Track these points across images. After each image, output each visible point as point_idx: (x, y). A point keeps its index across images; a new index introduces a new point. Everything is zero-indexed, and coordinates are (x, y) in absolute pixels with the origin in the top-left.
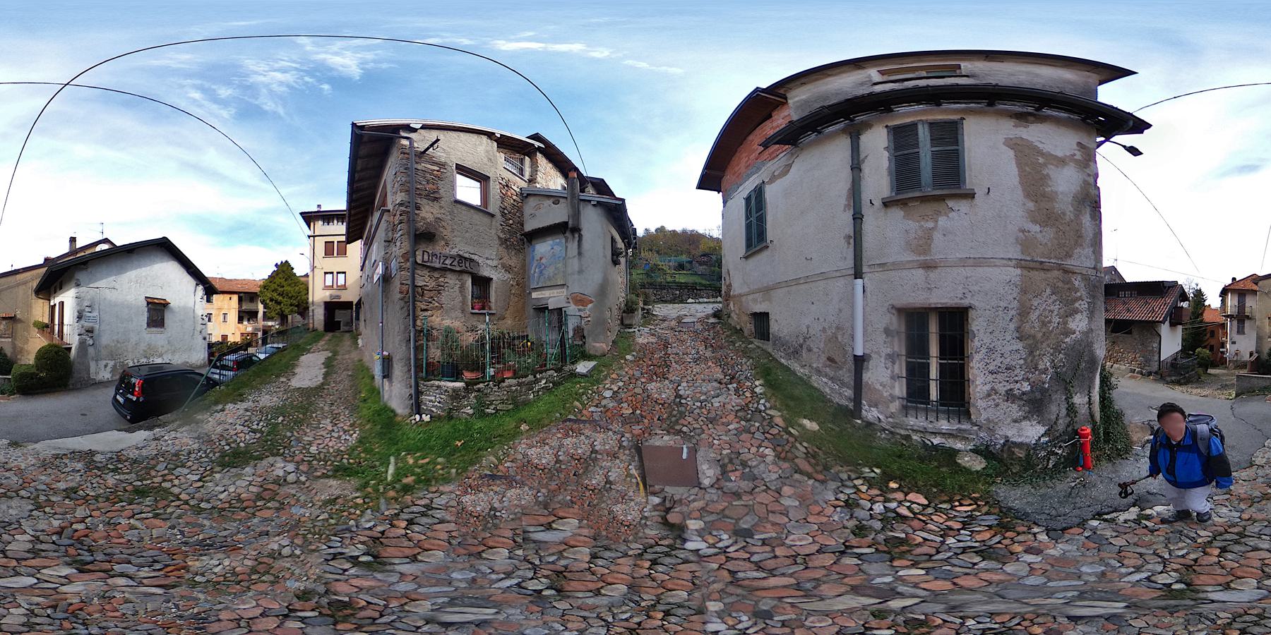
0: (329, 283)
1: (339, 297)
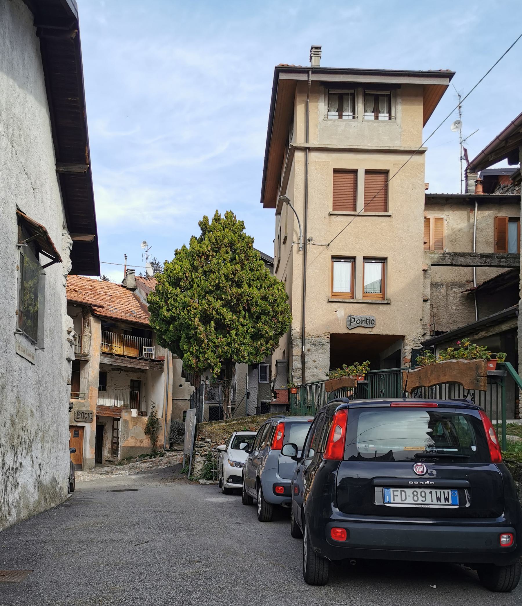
0: (342, 285)
1: (370, 322)
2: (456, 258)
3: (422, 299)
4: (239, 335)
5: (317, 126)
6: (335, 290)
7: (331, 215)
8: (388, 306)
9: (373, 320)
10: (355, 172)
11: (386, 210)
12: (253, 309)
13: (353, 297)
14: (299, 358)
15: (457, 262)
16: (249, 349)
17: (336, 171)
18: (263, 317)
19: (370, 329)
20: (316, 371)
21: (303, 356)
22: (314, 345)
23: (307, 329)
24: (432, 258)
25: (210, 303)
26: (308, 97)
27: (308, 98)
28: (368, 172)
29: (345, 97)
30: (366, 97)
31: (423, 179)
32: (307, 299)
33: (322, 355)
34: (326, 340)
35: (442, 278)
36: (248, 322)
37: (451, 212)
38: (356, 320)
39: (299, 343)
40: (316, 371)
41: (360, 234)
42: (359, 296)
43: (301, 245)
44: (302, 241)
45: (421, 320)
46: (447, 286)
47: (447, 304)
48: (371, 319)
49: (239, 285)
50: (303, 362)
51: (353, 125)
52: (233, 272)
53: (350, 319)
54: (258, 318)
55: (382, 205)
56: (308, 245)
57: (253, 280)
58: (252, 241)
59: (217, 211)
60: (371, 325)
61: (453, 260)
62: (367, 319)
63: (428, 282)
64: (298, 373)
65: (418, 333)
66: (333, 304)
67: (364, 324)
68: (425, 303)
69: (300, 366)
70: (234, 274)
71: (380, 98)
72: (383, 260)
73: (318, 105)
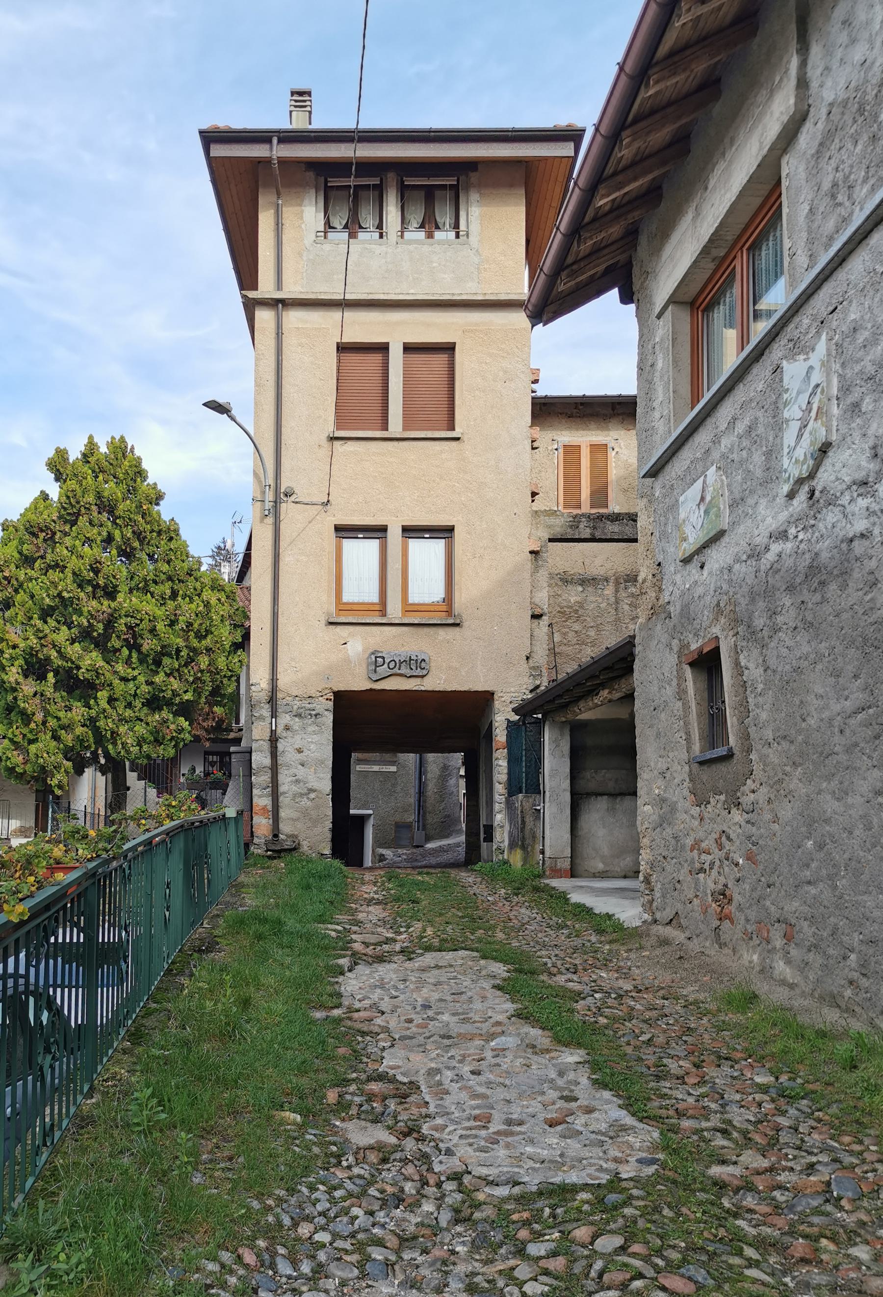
1: (417, 665)
2: (602, 525)
3: (530, 613)
4: (116, 700)
5: (300, 255)
6: (346, 598)
7: (332, 439)
8: (457, 629)
9: (424, 660)
10: (383, 348)
11: (452, 428)
12: (148, 644)
13: (383, 612)
14: (266, 746)
15: (605, 534)
16: (140, 729)
17: (342, 348)
18: (166, 661)
19: (418, 680)
20: (301, 772)
21: (274, 740)
22: (299, 715)
23: (283, 681)
24: (549, 527)
25: (41, 635)
26: (279, 195)
27: (278, 198)
28: (409, 348)
29: (362, 194)
30: (404, 192)
31: (526, 361)
32: (281, 620)
33: (316, 738)
34: (324, 707)
35: (608, 565)
36: (136, 673)
37: (623, 432)
38: (387, 661)
39: (266, 712)
40: (301, 772)
41: (390, 477)
42: (395, 611)
43: (269, 505)
44: (270, 496)
45: (528, 658)
46: (617, 583)
47: (618, 620)
48: (420, 658)
49: (111, 593)
50: (274, 754)
51: (377, 252)
52: (91, 565)
53: (376, 660)
54: (158, 663)
55: (444, 416)
56: (283, 505)
57: (155, 582)
58: (159, 497)
59: (91, 438)
60: (419, 672)
61: (595, 528)
62: (411, 659)
63: (543, 576)
64: (263, 778)
65: (521, 685)
66: (339, 629)
67: (404, 670)
68: (536, 621)
69: (267, 761)
70: (96, 572)
71: (438, 193)
72: (445, 532)
73: (302, 212)
